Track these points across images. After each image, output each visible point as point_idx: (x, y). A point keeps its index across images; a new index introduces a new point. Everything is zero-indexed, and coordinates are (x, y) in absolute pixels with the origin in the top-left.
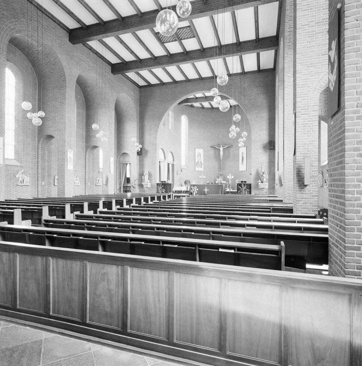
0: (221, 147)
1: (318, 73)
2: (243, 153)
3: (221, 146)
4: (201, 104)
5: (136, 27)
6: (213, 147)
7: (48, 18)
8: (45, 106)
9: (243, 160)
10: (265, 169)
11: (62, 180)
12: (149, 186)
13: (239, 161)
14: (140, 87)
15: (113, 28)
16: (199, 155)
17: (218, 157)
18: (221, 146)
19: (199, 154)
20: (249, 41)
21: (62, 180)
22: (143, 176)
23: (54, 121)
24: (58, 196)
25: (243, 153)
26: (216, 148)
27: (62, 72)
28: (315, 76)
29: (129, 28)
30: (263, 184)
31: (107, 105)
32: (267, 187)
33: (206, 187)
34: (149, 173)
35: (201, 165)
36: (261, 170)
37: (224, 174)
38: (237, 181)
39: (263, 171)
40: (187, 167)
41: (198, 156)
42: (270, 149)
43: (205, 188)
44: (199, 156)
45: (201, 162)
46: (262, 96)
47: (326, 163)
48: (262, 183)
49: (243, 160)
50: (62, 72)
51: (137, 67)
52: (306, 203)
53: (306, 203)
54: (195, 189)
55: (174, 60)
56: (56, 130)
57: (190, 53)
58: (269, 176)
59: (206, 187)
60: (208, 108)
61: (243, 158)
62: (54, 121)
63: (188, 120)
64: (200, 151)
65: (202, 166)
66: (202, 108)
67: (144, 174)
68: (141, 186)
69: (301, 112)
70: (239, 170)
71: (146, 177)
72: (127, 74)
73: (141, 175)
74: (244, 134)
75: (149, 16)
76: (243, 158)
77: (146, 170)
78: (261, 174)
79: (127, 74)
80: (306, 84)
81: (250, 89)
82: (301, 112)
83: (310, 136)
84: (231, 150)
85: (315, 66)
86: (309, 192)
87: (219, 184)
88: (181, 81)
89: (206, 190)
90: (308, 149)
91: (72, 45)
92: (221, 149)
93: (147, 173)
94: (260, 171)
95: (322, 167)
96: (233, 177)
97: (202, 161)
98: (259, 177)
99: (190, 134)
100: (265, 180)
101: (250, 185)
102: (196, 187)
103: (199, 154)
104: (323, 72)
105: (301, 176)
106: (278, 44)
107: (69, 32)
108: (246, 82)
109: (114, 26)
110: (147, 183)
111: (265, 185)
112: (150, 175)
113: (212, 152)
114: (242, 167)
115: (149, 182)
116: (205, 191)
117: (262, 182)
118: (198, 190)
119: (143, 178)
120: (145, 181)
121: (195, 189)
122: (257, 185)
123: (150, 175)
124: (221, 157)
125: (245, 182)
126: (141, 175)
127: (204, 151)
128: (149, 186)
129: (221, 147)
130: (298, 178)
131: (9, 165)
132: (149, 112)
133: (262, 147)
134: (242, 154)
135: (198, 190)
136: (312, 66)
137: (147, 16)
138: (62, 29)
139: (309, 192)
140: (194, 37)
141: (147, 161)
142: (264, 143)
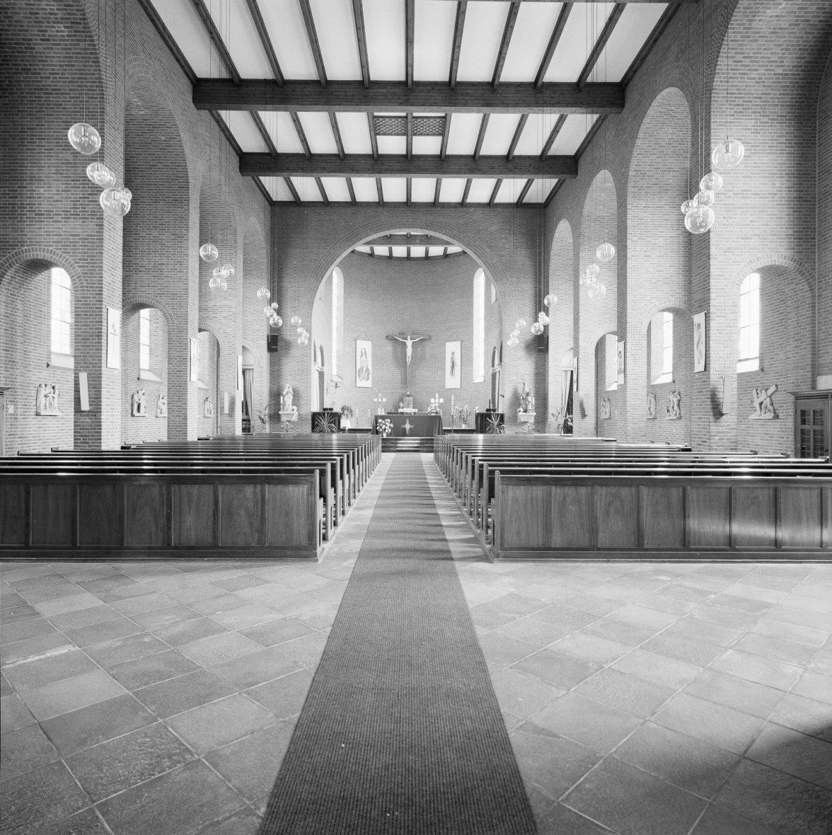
0: (409, 339)
1: (737, 262)
2: (453, 353)
3: (409, 337)
4: (372, 249)
5: (357, 105)
6: (390, 338)
7: (169, 52)
8: (131, 239)
9: (453, 367)
10: (529, 387)
11: (179, 404)
12: (294, 418)
13: (444, 369)
14: (272, 204)
15: (305, 97)
16: (364, 354)
17: (400, 359)
18: (409, 337)
19: (363, 352)
20: (529, 157)
21: (179, 404)
22: (282, 397)
23: (156, 274)
24: (75, 446)
25: (453, 353)
26: (396, 341)
27: (180, 169)
28: (733, 265)
29: (340, 105)
30: (527, 414)
31: (233, 242)
32: (532, 420)
33: (408, 421)
34: (294, 390)
35: (366, 375)
36: (524, 389)
37: (413, 394)
38: (477, 408)
39: (527, 390)
40: (342, 379)
41: (362, 355)
42: (540, 351)
43: (405, 423)
44: (364, 356)
45: (367, 369)
46: (523, 252)
47: (668, 379)
48: (524, 414)
49: (453, 367)
50: (180, 169)
51: (302, 169)
52: (723, 439)
53: (723, 439)
54: (387, 423)
55: (384, 167)
56: (163, 294)
57: (418, 160)
58: (535, 399)
59: (408, 421)
60: (381, 256)
61: (453, 363)
62: (156, 274)
63: (342, 279)
64: (365, 346)
65: (368, 377)
66: (371, 255)
67: (284, 393)
68: (275, 417)
69: (716, 313)
70: (445, 387)
71: (287, 400)
72: (262, 179)
73: (276, 395)
74: (519, 323)
75: (385, 90)
76: (453, 363)
77: (287, 385)
78: (524, 395)
79: (262, 179)
80: (722, 275)
81: (503, 236)
82: (716, 313)
83: (727, 347)
84: (428, 344)
85: (733, 252)
86: (726, 424)
87: (432, 414)
88: (366, 203)
89: (408, 426)
90: (724, 364)
91: (195, 111)
92: (409, 343)
93: (291, 391)
94: (520, 391)
95: (653, 386)
96: (442, 400)
97: (370, 367)
98: (517, 401)
99: (347, 308)
100: (530, 407)
101: (502, 416)
102: (389, 420)
103: (363, 352)
104: (742, 262)
105: (716, 402)
106: (577, 170)
107: (195, 82)
108: (493, 224)
109: (308, 93)
110: (289, 410)
111: (529, 417)
112: (296, 396)
113: (389, 348)
114: (452, 382)
115: (295, 410)
116: (405, 429)
117: (525, 411)
118: (392, 426)
119: (282, 402)
120: (286, 408)
121: (386, 425)
122: (514, 418)
123: (296, 396)
124: (409, 360)
125: (331, 409)
126: (276, 395)
127: (374, 346)
128: (294, 418)
129: (409, 339)
130: (713, 405)
131: (60, 368)
132: (295, 259)
133: (523, 346)
134: (451, 355)
135: (392, 426)
136: (730, 252)
137: (381, 90)
138: (185, 77)
139: (726, 424)
140: (440, 134)
141: (290, 365)
142: (527, 339)
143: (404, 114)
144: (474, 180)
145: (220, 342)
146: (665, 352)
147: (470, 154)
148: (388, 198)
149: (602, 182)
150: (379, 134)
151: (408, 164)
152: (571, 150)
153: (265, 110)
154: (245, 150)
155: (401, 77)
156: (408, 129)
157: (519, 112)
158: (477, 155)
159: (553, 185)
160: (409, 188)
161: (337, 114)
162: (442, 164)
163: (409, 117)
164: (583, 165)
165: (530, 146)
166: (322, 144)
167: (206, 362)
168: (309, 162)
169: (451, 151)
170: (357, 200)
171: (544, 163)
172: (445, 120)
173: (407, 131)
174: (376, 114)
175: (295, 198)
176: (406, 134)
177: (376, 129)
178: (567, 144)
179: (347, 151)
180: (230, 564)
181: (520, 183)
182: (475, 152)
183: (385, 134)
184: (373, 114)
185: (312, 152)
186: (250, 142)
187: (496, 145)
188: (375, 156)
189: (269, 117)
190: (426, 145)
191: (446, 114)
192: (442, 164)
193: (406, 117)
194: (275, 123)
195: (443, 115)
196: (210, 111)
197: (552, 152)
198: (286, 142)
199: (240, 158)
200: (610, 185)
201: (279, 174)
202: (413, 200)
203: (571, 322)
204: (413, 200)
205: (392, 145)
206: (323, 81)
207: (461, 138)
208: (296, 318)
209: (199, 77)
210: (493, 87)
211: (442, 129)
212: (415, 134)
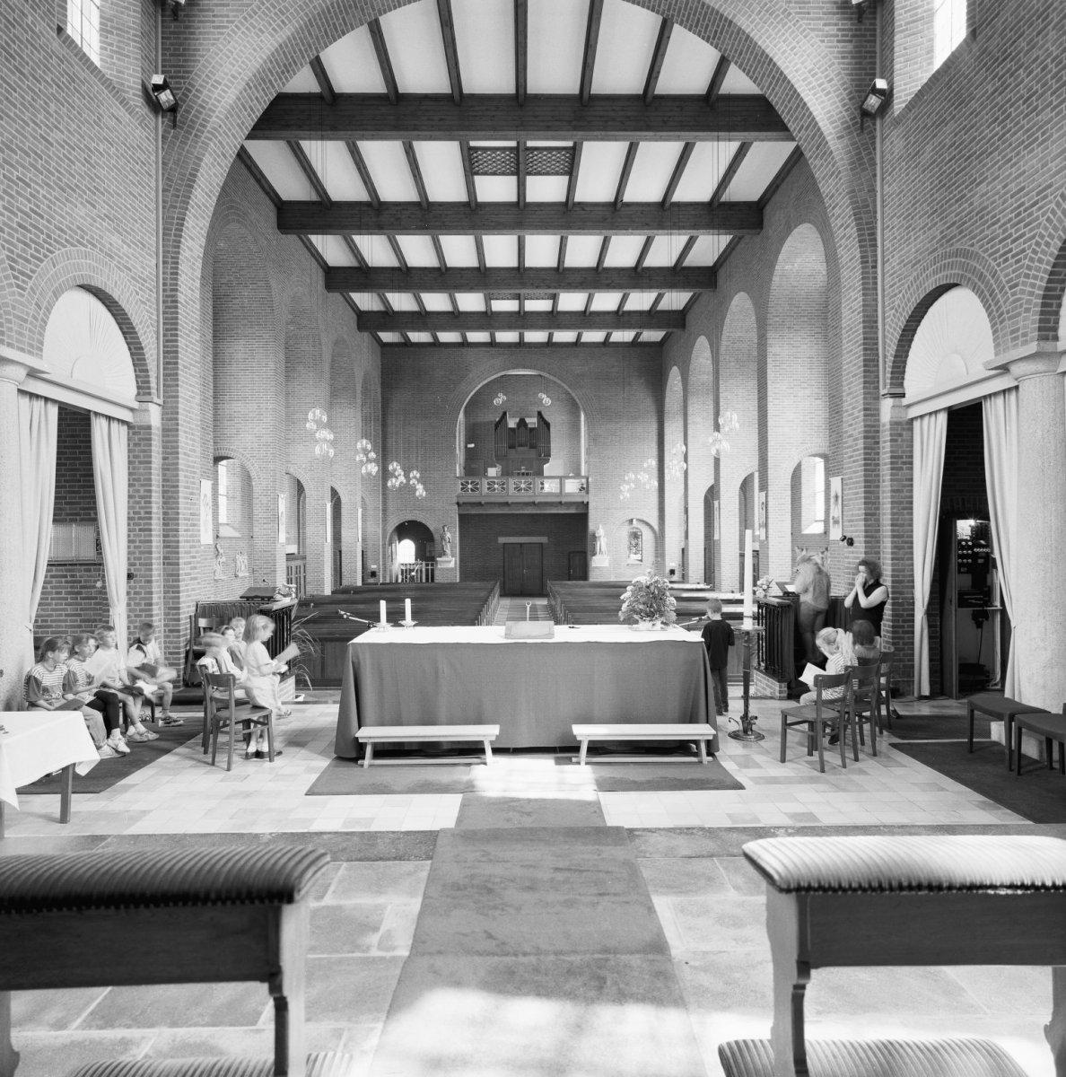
106: (716, 282)
143: (513, 144)
144: (614, 238)
145: (253, 474)
146: (818, 495)
147: (634, 92)
148: (491, 262)
149: (740, 305)
150: (477, 173)
151: (520, 216)
152: (753, 194)
153: (310, 139)
154: (284, 198)
155: (513, 263)
156: (520, 166)
157: (678, 139)
158: (650, 94)
159: (723, 246)
160: (521, 81)
161: (441, 237)
162: (569, 216)
163: (521, 148)
164: (773, 216)
165: (697, 187)
166: (394, 187)
167: (238, 505)
168: (405, 277)
169: (581, 196)
170: (400, 92)
171: (716, 213)
172: (573, 155)
173: (518, 169)
174: (473, 144)
175: (360, 263)
176: (517, 173)
177: (472, 165)
178: (749, 185)
179: (450, 264)
180: (204, 849)
181: (680, 240)
182: (598, 264)
183: (485, 174)
184: (468, 143)
185: (337, 90)
186: (291, 187)
187: (646, 188)
188: (473, 205)
189: (314, 149)
190: (546, 189)
191: (575, 143)
192: (569, 216)
193: (517, 149)
194: (320, 156)
195: (570, 144)
196: (341, 294)
197: (688, 262)
198: (342, 185)
199: (358, 316)
200: (749, 304)
201: (337, 231)
202: (529, 199)
203: (756, 441)
204: (529, 199)
205: (496, 189)
206: (425, 205)
207: (596, 182)
208: (318, 412)
209: (330, 265)
210: (644, 101)
211: (571, 169)
212: (530, 174)
